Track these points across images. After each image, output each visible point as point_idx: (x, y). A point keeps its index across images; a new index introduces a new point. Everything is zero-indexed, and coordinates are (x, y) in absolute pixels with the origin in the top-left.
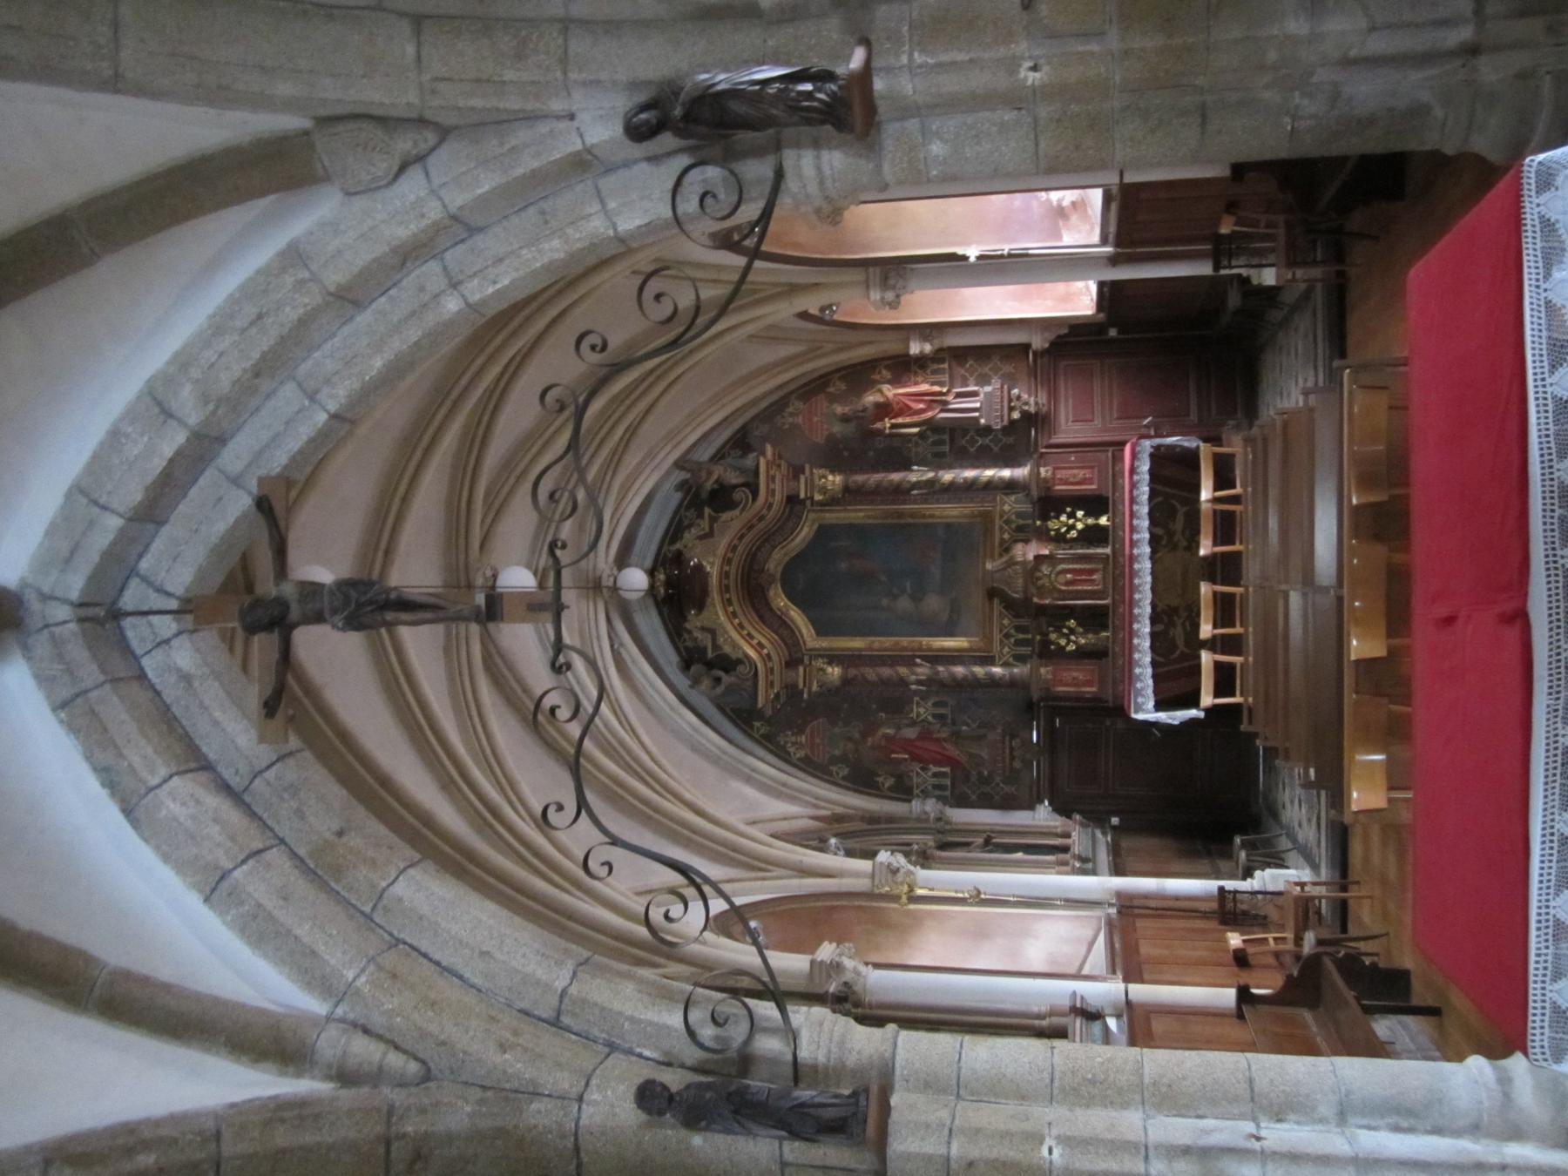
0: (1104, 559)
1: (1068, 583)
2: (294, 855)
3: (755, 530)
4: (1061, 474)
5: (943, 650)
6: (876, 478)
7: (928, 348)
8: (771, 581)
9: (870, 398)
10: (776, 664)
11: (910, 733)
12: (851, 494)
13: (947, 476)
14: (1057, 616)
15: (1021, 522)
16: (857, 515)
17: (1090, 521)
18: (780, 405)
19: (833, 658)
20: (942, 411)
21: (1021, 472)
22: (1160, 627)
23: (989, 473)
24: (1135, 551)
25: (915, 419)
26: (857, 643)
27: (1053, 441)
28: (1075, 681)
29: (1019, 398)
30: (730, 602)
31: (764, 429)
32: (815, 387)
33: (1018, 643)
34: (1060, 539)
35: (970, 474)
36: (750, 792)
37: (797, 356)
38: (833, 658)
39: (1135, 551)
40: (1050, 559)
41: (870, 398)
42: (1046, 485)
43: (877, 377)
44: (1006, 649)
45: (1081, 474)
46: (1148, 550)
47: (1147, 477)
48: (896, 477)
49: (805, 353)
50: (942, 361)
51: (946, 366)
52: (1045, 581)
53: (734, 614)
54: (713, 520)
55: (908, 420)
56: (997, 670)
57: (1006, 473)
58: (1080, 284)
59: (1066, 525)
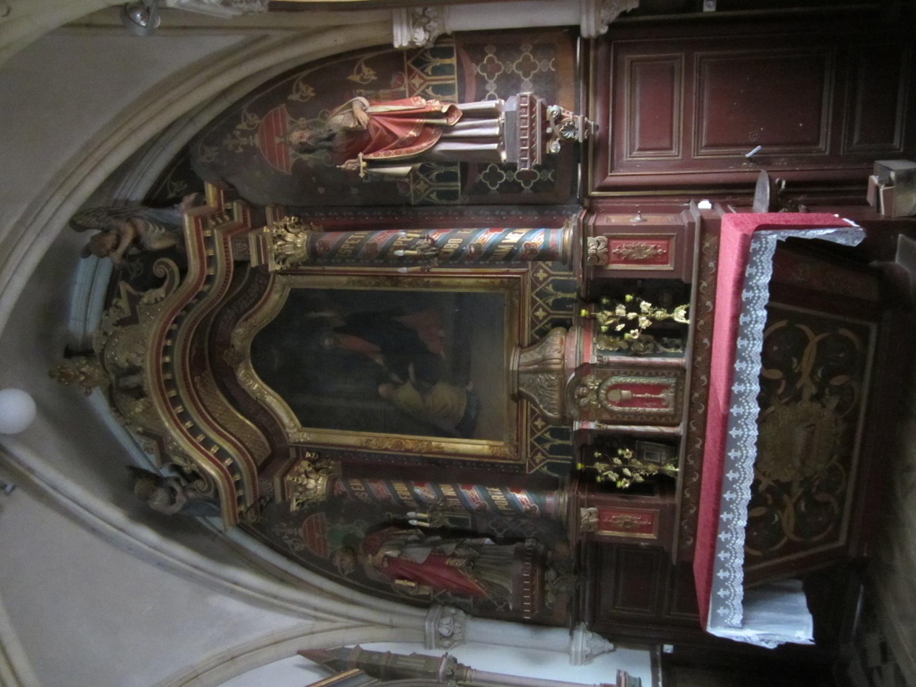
1: (623, 402)
3: (185, 323)
5: (457, 454)
7: (421, 37)
8: (240, 358)
9: (340, 119)
10: (244, 475)
14: (607, 444)
15: (561, 295)
17: (660, 314)
18: (228, 120)
19: (322, 457)
20: (443, 140)
21: (560, 237)
22: (760, 511)
23: (513, 237)
24: (734, 410)
25: (404, 153)
26: (351, 439)
27: (610, 180)
29: (559, 119)
30: (176, 401)
31: (211, 153)
32: (273, 92)
33: (554, 450)
35: (486, 237)
36: (234, 606)
37: (231, 52)
38: (322, 457)
39: (734, 410)
40: (603, 370)
41: (340, 119)
43: (355, 78)
44: (539, 457)
46: (756, 409)
47: (766, 294)
49: (245, 46)
50: (447, 53)
51: (453, 61)
52: (592, 399)
53: (184, 417)
54: (133, 301)
55: (393, 155)
57: (538, 238)
58: (814, 387)
59: (623, 320)
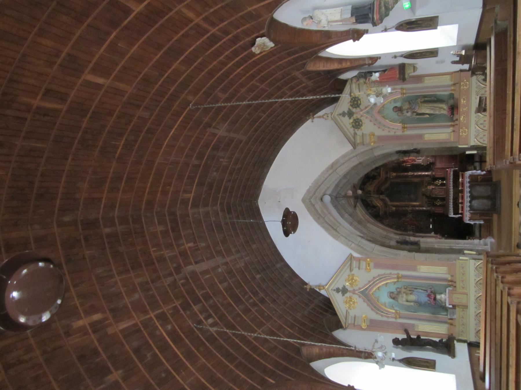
0: (445, 189)
2: (344, 227)
4: (437, 174)
6: (402, 174)
11: (408, 220)
12: (397, 177)
13: (416, 174)
14: (436, 199)
16: (399, 180)
19: (394, 206)
26: (398, 203)
28: (439, 210)
34: (436, 185)
35: (420, 173)
38: (394, 206)
42: (434, 176)
45: (440, 174)
48: (406, 174)
56: (424, 208)
57: (426, 173)
